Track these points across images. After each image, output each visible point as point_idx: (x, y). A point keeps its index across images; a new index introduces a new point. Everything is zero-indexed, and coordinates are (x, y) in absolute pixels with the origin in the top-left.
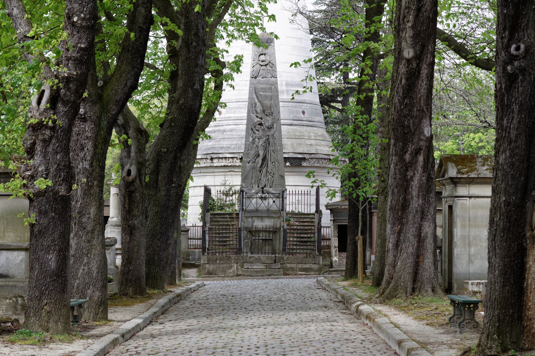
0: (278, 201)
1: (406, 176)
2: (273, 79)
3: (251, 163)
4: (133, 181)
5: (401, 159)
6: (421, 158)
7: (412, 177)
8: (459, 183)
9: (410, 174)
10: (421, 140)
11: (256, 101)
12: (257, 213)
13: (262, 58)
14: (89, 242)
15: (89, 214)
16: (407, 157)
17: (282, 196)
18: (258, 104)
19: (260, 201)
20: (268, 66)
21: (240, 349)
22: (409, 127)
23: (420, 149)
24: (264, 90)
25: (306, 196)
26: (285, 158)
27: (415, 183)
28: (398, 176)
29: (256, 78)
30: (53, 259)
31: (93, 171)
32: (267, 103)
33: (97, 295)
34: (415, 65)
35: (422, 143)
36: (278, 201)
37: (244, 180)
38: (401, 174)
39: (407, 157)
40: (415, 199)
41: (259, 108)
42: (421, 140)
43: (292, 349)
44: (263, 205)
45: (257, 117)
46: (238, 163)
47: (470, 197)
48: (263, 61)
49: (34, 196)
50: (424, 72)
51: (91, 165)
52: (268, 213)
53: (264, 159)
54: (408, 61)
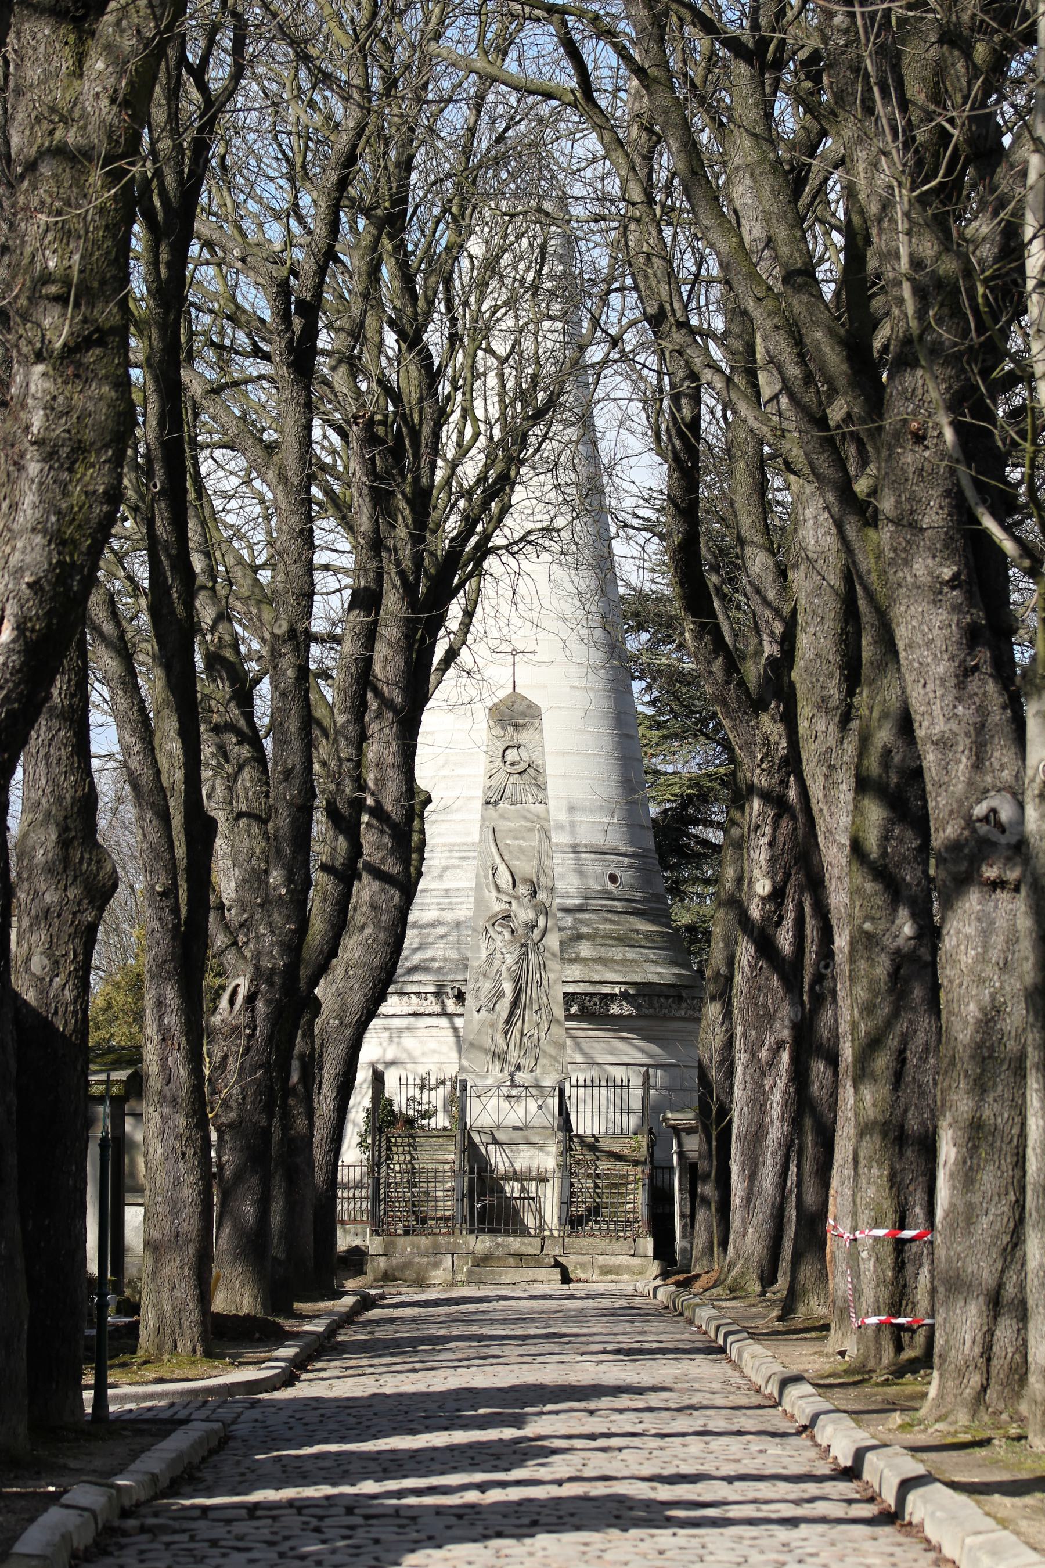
1: (762, 1085)
2: (539, 808)
3: (483, 1012)
5: (754, 1056)
11: (498, 860)
13: (512, 755)
18: (502, 868)
19: (505, 1105)
20: (526, 776)
22: (765, 1005)
25: (603, 1091)
26: (566, 995)
28: (749, 1086)
29: (497, 803)
33: (935, 394)
38: (754, 1083)
39: (764, 1054)
40: (777, 1123)
41: (504, 879)
45: (499, 900)
48: (513, 764)
49: (934, 343)
53: (515, 1003)
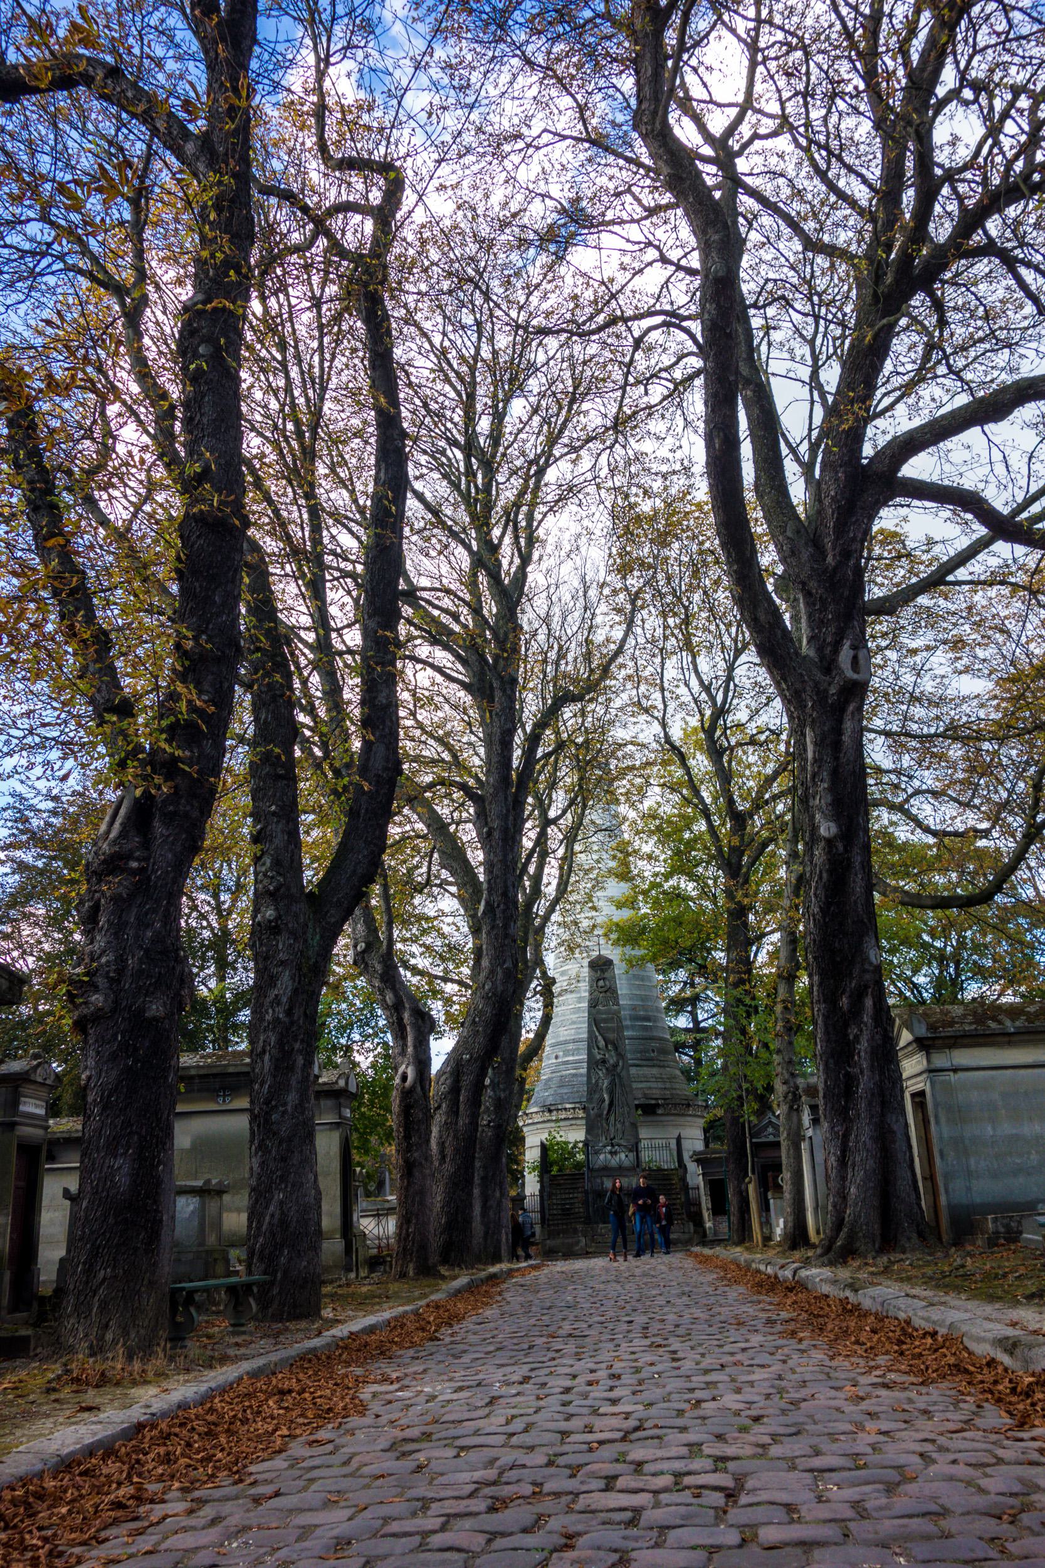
0: (632, 1156)
1: (846, 1035)
4: (413, 1087)
6: (869, 1002)
7: (857, 1037)
8: (933, 1047)
9: (853, 1031)
10: (865, 971)
12: (606, 1170)
14: (284, 1159)
15: (285, 1104)
16: (844, 1002)
17: (635, 1148)
21: (568, 1383)
23: (866, 987)
24: (605, 1021)
27: (863, 1045)
30: (126, 1169)
31: (292, 1023)
32: (611, 1036)
34: (841, 848)
35: (867, 976)
36: (632, 1156)
37: (588, 1132)
39: (844, 1002)
42: (865, 971)
43: (708, 1378)
44: (614, 1162)
46: (581, 1114)
47: (955, 1070)
50: (857, 860)
51: (289, 1012)
52: (621, 1170)
53: (611, 1104)
54: (829, 842)
